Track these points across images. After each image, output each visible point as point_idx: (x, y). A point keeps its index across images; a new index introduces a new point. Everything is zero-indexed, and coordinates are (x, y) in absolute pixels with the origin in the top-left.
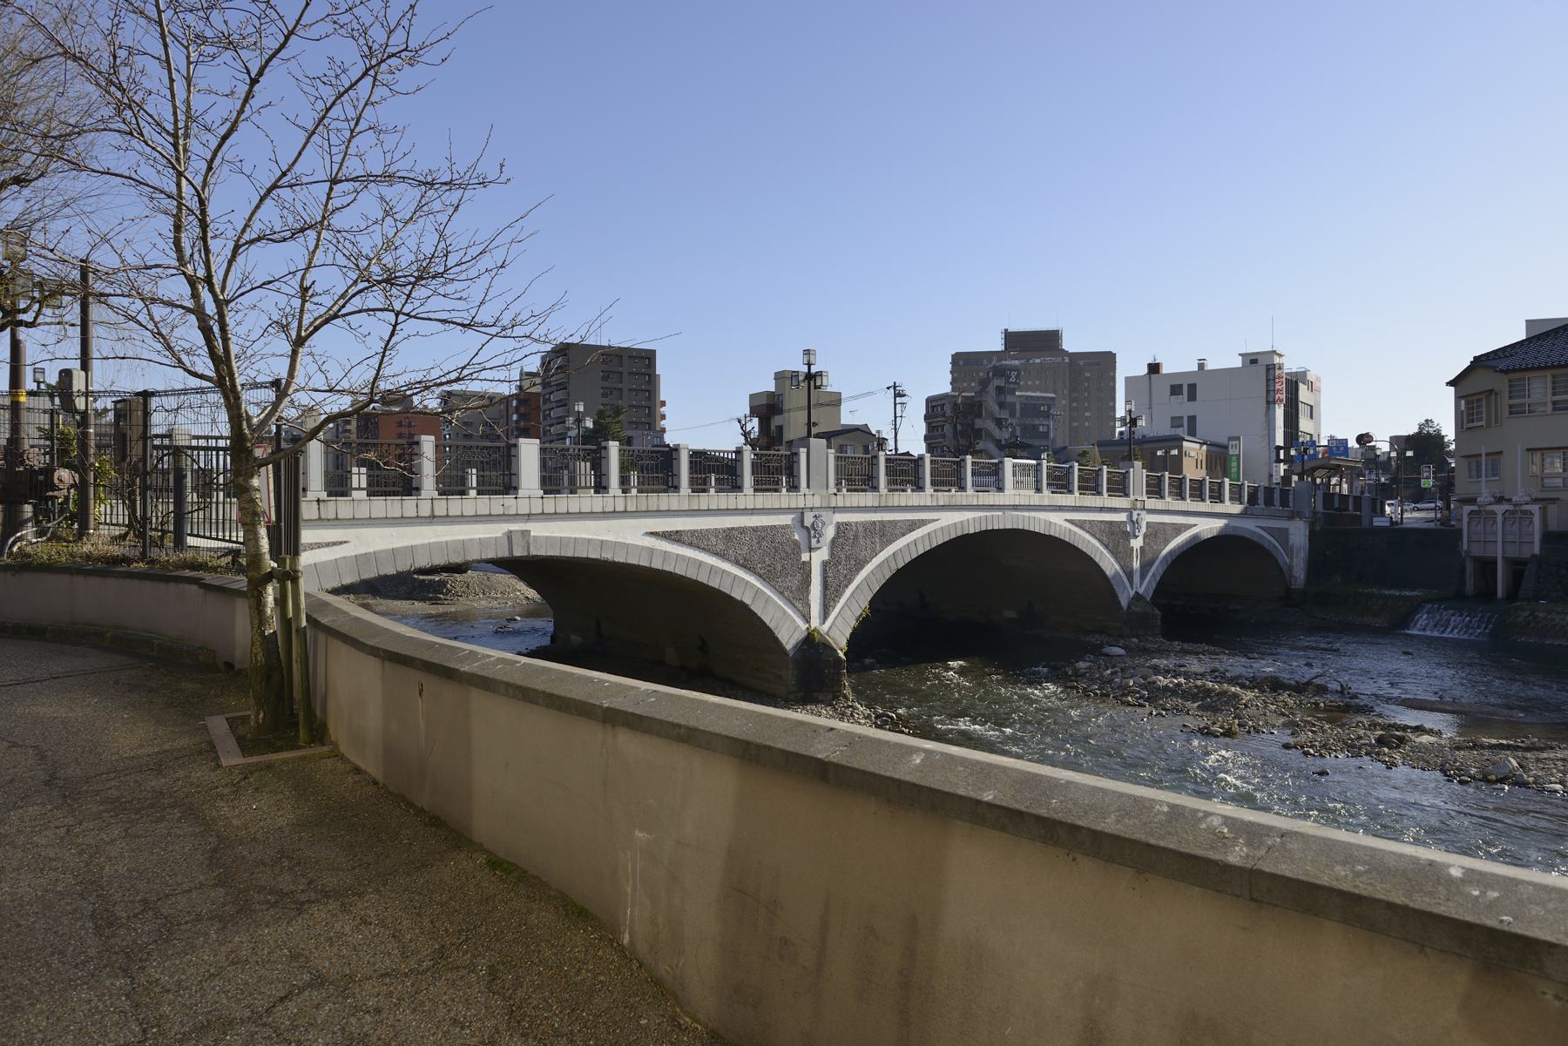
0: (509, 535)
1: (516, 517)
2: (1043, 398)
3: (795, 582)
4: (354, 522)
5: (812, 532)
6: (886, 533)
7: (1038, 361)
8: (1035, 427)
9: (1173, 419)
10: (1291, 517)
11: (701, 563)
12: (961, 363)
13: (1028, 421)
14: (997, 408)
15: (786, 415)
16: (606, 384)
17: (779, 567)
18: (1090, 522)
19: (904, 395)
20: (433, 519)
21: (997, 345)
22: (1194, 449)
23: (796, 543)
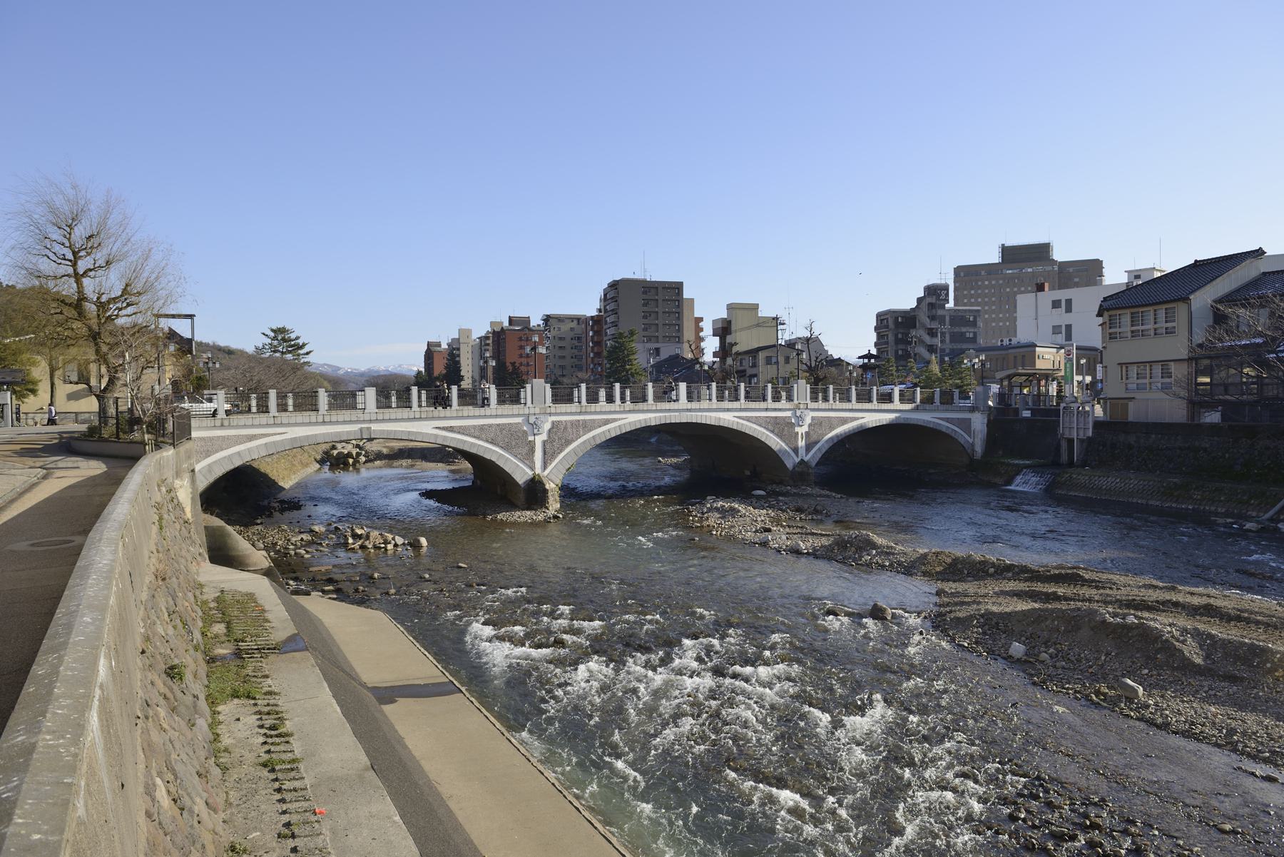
0: (361, 429)
1: (364, 421)
2: (969, 310)
3: (525, 450)
4: (289, 425)
5: (800, 419)
6: (587, 426)
7: (1030, 270)
8: (963, 334)
9: (1054, 327)
10: (973, 409)
11: (465, 441)
12: (962, 274)
13: (957, 330)
14: (928, 320)
15: (733, 334)
16: (645, 309)
17: (514, 443)
18: (756, 417)
19: (784, 324)
20: (324, 423)
21: (994, 257)
22: (1049, 353)
23: (525, 432)
